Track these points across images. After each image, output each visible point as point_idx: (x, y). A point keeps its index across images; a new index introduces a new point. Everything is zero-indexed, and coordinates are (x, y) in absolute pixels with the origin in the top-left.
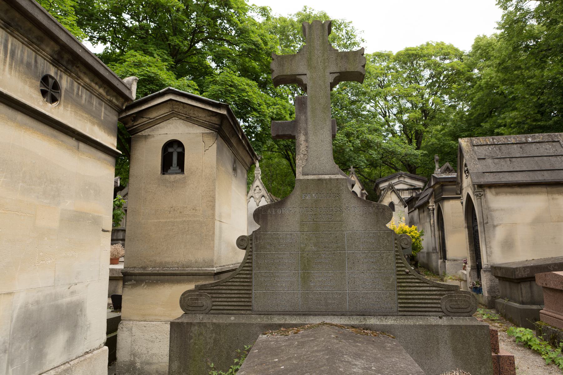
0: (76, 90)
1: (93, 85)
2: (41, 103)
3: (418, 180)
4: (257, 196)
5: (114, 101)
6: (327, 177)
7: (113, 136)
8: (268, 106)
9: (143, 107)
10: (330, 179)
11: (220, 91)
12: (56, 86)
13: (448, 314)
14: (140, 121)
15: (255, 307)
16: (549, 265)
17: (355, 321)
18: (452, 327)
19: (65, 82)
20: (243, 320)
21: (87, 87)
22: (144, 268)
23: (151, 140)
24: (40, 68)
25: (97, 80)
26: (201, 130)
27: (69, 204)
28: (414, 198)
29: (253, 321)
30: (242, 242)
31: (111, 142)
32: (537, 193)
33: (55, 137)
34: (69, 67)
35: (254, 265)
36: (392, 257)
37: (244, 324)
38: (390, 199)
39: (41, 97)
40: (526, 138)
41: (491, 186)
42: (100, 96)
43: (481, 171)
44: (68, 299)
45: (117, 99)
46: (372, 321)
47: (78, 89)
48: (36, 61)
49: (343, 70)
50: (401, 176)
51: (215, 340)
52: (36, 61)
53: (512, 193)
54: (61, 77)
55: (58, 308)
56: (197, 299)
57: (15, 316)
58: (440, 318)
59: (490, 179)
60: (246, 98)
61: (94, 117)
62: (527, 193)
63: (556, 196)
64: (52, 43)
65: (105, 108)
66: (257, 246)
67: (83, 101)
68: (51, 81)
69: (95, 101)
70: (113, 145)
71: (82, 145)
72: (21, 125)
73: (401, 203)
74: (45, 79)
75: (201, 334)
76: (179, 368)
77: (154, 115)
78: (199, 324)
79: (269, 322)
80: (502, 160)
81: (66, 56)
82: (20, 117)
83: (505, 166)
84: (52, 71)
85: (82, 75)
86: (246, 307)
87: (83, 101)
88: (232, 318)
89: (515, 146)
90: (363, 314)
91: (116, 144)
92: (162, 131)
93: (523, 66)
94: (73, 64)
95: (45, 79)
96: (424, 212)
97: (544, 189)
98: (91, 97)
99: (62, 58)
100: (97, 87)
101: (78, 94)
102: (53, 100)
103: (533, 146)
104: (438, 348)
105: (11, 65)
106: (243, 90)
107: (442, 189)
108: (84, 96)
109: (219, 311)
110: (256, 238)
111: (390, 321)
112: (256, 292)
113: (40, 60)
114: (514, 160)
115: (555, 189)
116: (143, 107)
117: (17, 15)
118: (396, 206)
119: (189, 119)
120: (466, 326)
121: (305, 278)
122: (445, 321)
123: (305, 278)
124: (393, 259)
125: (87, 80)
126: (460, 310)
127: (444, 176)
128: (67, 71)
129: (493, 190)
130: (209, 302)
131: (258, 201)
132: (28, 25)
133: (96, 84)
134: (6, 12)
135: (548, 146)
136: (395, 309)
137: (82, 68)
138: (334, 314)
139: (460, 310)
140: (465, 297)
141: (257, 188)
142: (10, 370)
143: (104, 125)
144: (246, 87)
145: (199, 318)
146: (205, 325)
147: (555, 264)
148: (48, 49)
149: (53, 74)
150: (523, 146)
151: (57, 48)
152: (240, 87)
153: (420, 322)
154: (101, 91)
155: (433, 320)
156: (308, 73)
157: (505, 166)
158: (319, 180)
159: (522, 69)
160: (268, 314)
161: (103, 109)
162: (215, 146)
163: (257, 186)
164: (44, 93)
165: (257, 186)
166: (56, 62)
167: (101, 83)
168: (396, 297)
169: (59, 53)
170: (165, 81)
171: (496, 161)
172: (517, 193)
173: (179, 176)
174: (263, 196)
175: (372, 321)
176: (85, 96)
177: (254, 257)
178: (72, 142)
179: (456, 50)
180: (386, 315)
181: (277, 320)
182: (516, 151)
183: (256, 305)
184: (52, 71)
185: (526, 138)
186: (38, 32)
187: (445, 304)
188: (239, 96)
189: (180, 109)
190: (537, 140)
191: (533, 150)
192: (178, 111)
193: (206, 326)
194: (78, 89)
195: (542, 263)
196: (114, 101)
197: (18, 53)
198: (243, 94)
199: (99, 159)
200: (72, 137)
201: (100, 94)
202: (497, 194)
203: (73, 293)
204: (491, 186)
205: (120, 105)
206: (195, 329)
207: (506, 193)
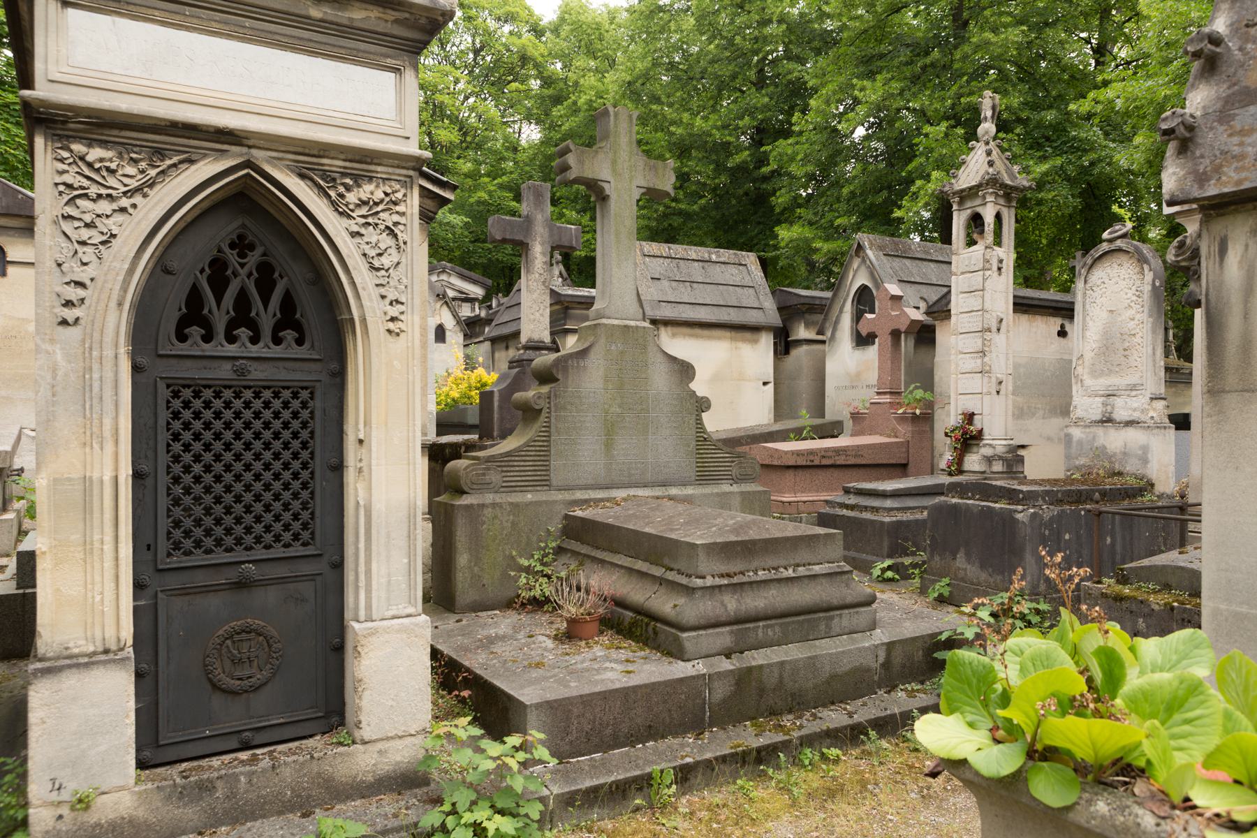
3: (475, 282)
10: (637, 327)
13: (736, 480)
15: (554, 483)
16: (742, 437)
17: (658, 492)
18: (742, 493)
20: (542, 496)
28: (481, 319)
29: (554, 498)
32: (719, 338)
35: (553, 429)
37: (546, 502)
38: (437, 317)
40: (710, 253)
41: (667, 323)
43: (656, 298)
46: (674, 491)
49: (651, 186)
50: (444, 271)
51: (513, 523)
53: (691, 336)
56: (484, 474)
59: (667, 312)
62: (709, 338)
63: (740, 344)
66: (556, 405)
73: (457, 328)
75: (495, 517)
76: (470, 561)
78: (494, 505)
79: (573, 498)
80: (681, 285)
83: (685, 294)
86: (544, 483)
88: (529, 496)
89: (696, 264)
93: (664, 99)
96: (507, 348)
97: (727, 334)
103: (718, 268)
107: (565, 313)
109: (511, 489)
110: (555, 395)
111: (689, 491)
112: (555, 463)
114: (695, 285)
115: (740, 335)
118: (448, 334)
121: (609, 445)
122: (735, 488)
123: (609, 445)
127: (570, 292)
129: (669, 329)
130: (499, 477)
135: (733, 270)
146: (500, 505)
147: (749, 436)
150: (706, 265)
155: (726, 488)
156: (612, 181)
157: (685, 294)
159: (663, 103)
171: (674, 284)
172: (697, 336)
175: (674, 491)
177: (553, 420)
179: (531, 14)
182: (696, 271)
185: (710, 253)
190: (722, 259)
191: (717, 273)
193: (501, 507)
195: (734, 435)
202: (674, 335)
204: (667, 323)
206: (488, 512)
207: (684, 335)
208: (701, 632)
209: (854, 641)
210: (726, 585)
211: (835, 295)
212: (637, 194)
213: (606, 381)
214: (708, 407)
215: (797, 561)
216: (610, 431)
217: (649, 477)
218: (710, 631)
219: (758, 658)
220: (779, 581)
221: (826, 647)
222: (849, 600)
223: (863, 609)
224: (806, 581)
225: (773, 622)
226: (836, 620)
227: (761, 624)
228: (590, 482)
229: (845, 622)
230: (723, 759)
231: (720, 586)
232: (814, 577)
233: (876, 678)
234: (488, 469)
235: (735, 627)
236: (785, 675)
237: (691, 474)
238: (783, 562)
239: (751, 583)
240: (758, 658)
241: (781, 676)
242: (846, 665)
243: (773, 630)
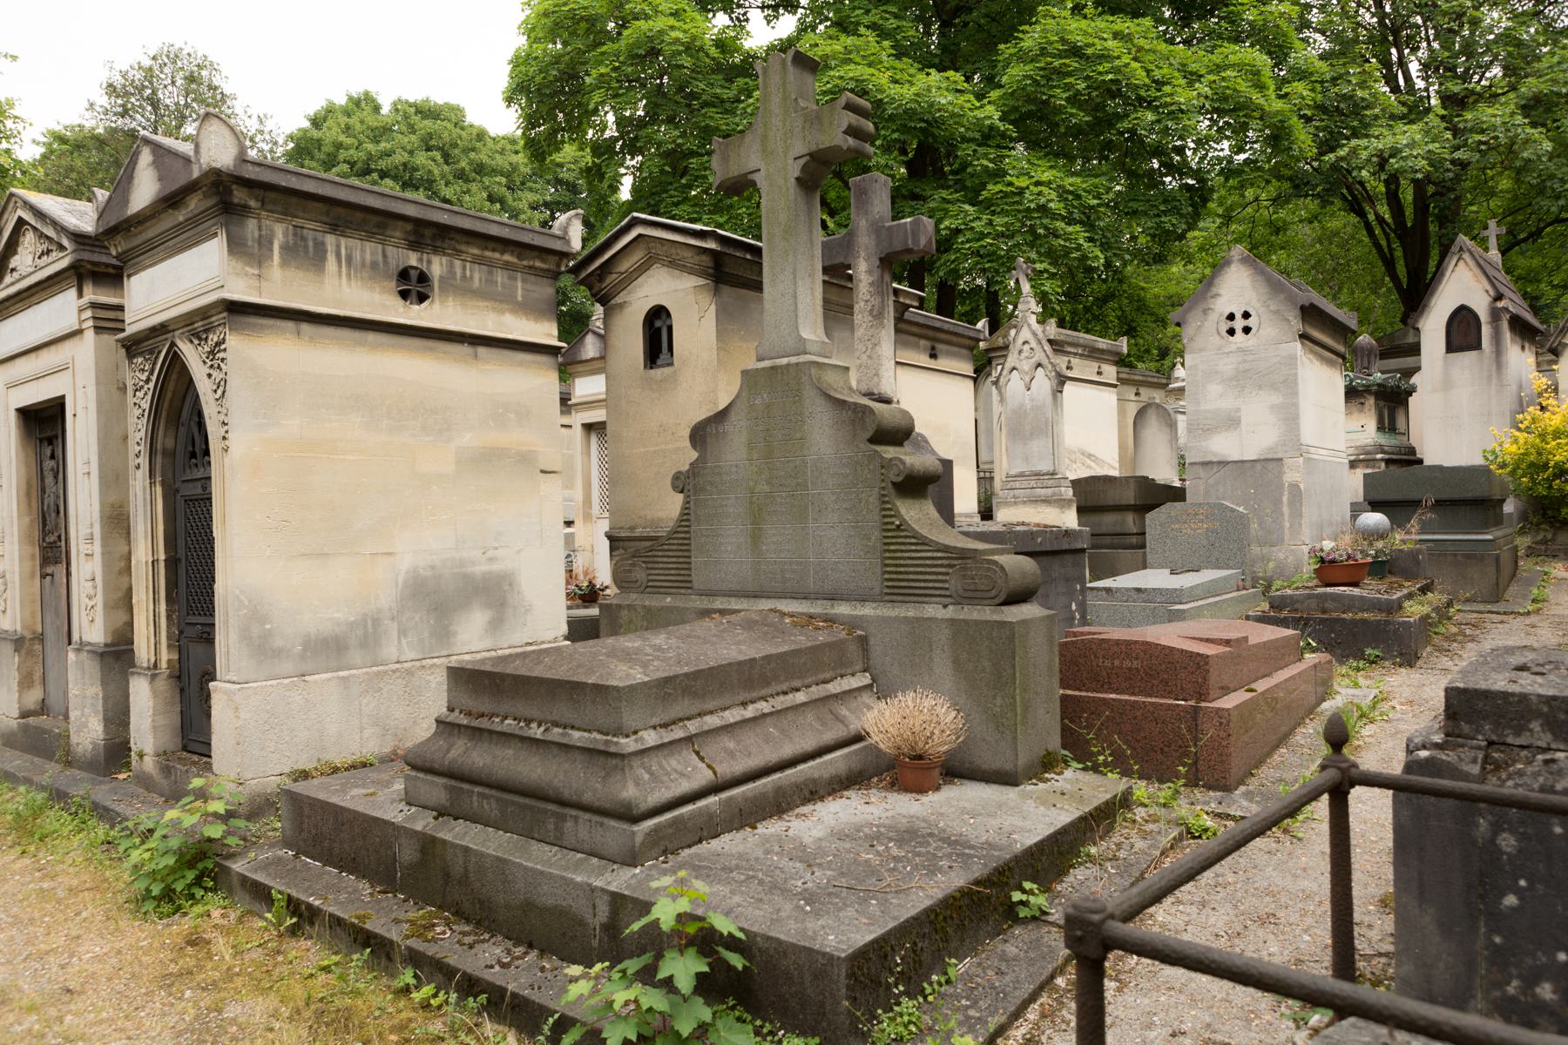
0: (458, 271)
1: (488, 254)
2: (401, 310)
4: (1026, 366)
5: (538, 264)
6: (784, 361)
7: (549, 320)
8: (1193, 78)
9: (607, 256)
11: (1031, 77)
12: (423, 278)
14: (611, 279)
15: (696, 585)
18: (952, 622)
19: (437, 267)
21: (478, 261)
22: (632, 529)
23: (628, 310)
24: (392, 262)
25: (492, 245)
26: (693, 281)
27: (468, 439)
29: (690, 605)
30: (681, 483)
31: (545, 332)
33: (431, 349)
34: (439, 243)
35: (692, 517)
36: (874, 500)
39: (400, 302)
42: (507, 266)
44: (485, 568)
45: (543, 261)
47: (464, 268)
48: (385, 256)
49: (814, 148)
52: (385, 256)
54: (429, 262)
55: (466, 577)
57: (401, 581)
58: (945, 606)
60: (1110, 76)
61: (505, 301)
64: (400, 223)
65: (524, 281)
67: (476, 283)
68: (414, 274)
69: (500, 277)
70: (550, 335)
71: (482, 350)
72: (374, 347)
74: (404, 275)
77: (625, 265)
81: (428, 232)
82: (372, 337)
84: (413, 259)
85: (463, 248)
86: (684, 584)
87: (476, 283)
90: (833, 597)
91: (555, 332)
92: (641, 293)
94: (443, 238)
95: (404, 275)
98: (490, 273)
99: (423, 236)
100: (497, 255)
101: (464, 276)
102: (422, 298)
104: (931, 659)
105: (349, 275)
106: (1103, 57)
108: (476, 276)
113: (390, 250)
116: (607, 256)
117: (341, 210)
119: (673, 264)
120: (976, 622)
121: (756, 538)
122: (950, 612)
123: (756, 538)
124: (877, 503)
125: (476, 251)
126: (978, 594)
128: (436, 250)
131: (1027, 379)
132: (359, 215)
133: (494, 250)
134: (328, 214)
136: (877, 591)
137: (458, 237)
138: (794, 596)
139: (978, 594)
140: (988, 569)
141: (1026, 347)
142: (404, 642)
143: (528, 308)
144: (1111, 44)
145: (634, 598)
148: (398, 234)
149: (414, 263)
151: (409, 227)
152: (1089, 51)
153: (909, 611)
154: (507, 257)
155: (933, 610)
158: (772, 368)
160: (711, 594)
161: (519, 284)
162: (713, 307)
163: (1025, 343)
164: (404, 295)
165: (1025, 343)
166: (415, 245)
167: (500, 247)
168: (878, 570)
169: (415, 232)
170: (881, 91)
173: (667, 370)
174: (1039, 365)
176: (477, 275)
178: (465, 349)
180: (863, 600)
181: (719, 603)
183: (698, 581)
184: (413, 259)
186: (375, 219)
187: (954, 584)
188: (1088, 78)
189: (659, 249)
192: (656, 255)
194: (464, 268)
196: (538, 264)
197: (357, 256)
198: (1101, 69)
199: (520, 364)
200: (462, 342)
201: (507, 263)
203: (491, 560)
205: (553, 267)
206: (624, 613)
208: (421, 775)
209: (577, 867)
210: (466, 727)
211: (518, 303)
212: (795, 170)
213: (750, 449)
214: (677, 477)
215: (556, 718)
216: (757, 517)
217: (811, 584)
218: (429, 777)
219: (458, 833)
220: (523, 739)
221: (539, 858)
222: (588, 797)
223: (613, 823)
224: (555, 750)
225: (493, 792)
226: (569, 824)
227: (477, 789)
228: (734, 586)
229: (583, 832)
230: (337, 922)
231: (459, 726)
232: (566, 748)
233: (595, 943)
234: (634, 565)
235: (453, 783)
236: (471, 867)
237: (875, 583)
238: (535, 713)
239: (491, 732)
240: (458, 833)
241: (466, 868)
242: (548, 896)
243: (488, 804)
